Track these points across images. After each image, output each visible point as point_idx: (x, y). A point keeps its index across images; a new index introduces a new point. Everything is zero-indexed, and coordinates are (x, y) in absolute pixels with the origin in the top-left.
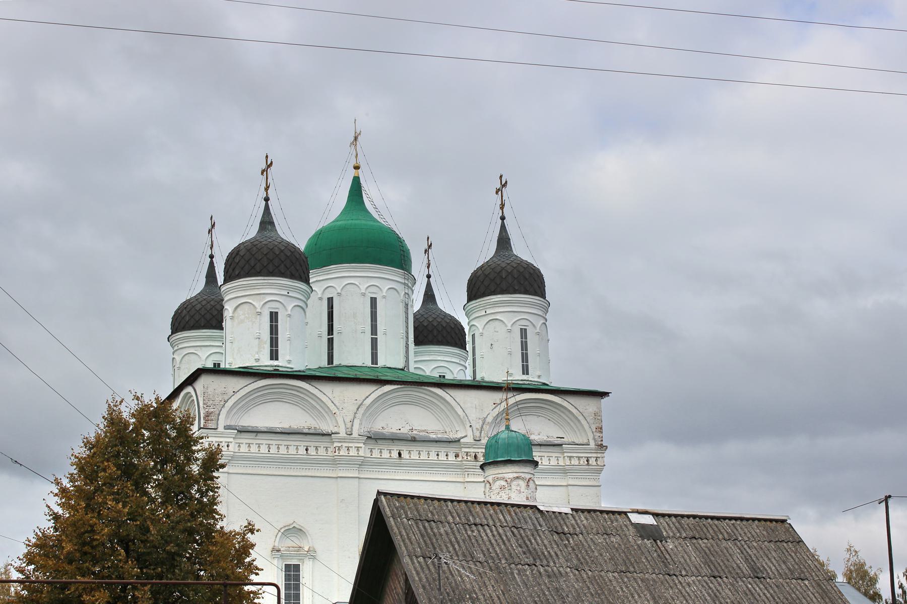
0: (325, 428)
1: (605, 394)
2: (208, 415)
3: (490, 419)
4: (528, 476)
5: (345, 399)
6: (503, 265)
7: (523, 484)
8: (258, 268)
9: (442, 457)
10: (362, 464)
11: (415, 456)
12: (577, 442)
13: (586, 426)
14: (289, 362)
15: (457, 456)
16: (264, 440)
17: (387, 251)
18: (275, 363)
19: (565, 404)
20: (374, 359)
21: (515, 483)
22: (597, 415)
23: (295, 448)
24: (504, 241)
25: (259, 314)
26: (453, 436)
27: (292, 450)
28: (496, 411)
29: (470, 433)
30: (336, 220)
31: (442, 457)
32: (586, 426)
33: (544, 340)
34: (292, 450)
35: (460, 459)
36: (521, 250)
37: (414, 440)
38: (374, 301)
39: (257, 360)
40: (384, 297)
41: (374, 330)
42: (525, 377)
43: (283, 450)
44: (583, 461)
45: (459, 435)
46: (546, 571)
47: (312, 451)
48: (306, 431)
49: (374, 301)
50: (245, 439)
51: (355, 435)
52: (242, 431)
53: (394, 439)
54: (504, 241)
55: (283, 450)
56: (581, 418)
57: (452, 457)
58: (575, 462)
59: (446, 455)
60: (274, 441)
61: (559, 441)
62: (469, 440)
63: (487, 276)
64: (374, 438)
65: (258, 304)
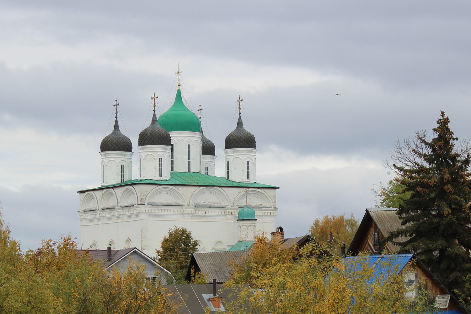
0: (180, 203)
1: (279, 188)
2: (141, 200)
3: (237, 199)
4: (254, 225)
5: (187, 193)
6: (241, 136)
7: (252, 227)
8: (155, 141)
9: (220, 213)
10: (192, 216)
11: (210, 213)
12: (267, 206)
13: (271, 201)
14: (166, 177)
15: (225, 212)
16: (160, 208)
17: (192, 125)
18: (161, 178)
19: (263, 192)
20: (189, 170)
21: (250, 227)
22: (275, 196)
23: (170, 210)
24: (240, 124)
25: (155, 159)
26: (223, 205)
27: (169, 212)
28: (240, 195)
29: (230, 205)
30: (171, 110)
31: (220, 213)
32: (271, 201)
33: (255, 164)
34: (169, 212)
35: (226, 213)
36: (248, 128)
37: (210, 207)
38: (189, 146)
39: (155, 177)
40: (193, 144)
41: (189, 158)
42: (248, 180)
43: (166, 212)
44: (269, 214)
45: (226, 205)
46: (426, 294)
47: (176, 212)
48: (173, 204)
49: (189, 146)
50: (154, 208)
51: (191, 206)
52: (153, 205)
53: (204, 206)
54: (240, 124)
55: (166, 212)
56: (269, 197)
57: (223, 213)
58: (266, 214)
59: (220, 212)
60: (163, 208)
61: (260, 206)
62: (229, 207)
63: (234, 140)
64: (197, 206)
65: (155, 155)
